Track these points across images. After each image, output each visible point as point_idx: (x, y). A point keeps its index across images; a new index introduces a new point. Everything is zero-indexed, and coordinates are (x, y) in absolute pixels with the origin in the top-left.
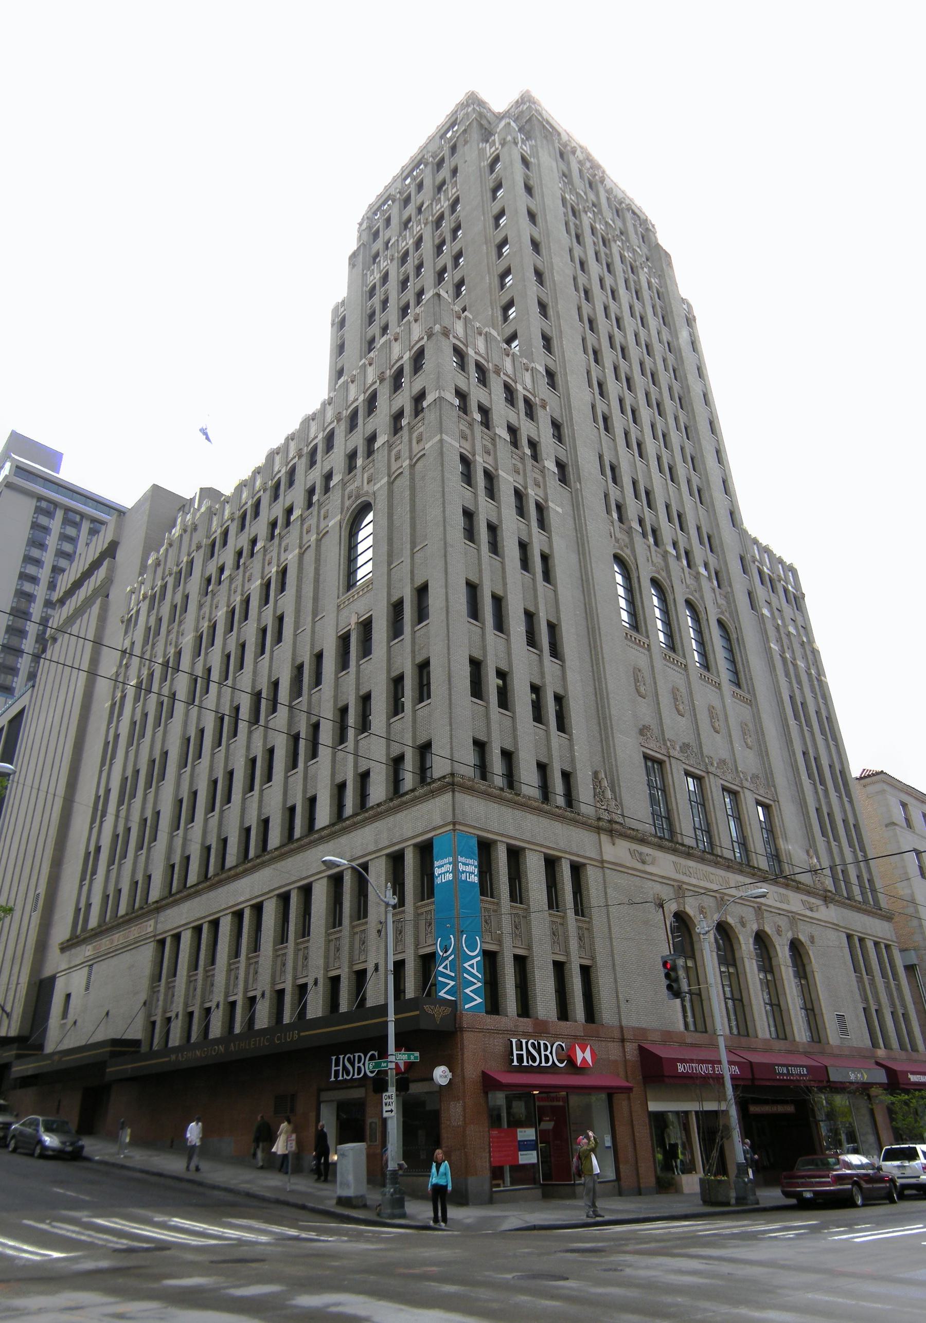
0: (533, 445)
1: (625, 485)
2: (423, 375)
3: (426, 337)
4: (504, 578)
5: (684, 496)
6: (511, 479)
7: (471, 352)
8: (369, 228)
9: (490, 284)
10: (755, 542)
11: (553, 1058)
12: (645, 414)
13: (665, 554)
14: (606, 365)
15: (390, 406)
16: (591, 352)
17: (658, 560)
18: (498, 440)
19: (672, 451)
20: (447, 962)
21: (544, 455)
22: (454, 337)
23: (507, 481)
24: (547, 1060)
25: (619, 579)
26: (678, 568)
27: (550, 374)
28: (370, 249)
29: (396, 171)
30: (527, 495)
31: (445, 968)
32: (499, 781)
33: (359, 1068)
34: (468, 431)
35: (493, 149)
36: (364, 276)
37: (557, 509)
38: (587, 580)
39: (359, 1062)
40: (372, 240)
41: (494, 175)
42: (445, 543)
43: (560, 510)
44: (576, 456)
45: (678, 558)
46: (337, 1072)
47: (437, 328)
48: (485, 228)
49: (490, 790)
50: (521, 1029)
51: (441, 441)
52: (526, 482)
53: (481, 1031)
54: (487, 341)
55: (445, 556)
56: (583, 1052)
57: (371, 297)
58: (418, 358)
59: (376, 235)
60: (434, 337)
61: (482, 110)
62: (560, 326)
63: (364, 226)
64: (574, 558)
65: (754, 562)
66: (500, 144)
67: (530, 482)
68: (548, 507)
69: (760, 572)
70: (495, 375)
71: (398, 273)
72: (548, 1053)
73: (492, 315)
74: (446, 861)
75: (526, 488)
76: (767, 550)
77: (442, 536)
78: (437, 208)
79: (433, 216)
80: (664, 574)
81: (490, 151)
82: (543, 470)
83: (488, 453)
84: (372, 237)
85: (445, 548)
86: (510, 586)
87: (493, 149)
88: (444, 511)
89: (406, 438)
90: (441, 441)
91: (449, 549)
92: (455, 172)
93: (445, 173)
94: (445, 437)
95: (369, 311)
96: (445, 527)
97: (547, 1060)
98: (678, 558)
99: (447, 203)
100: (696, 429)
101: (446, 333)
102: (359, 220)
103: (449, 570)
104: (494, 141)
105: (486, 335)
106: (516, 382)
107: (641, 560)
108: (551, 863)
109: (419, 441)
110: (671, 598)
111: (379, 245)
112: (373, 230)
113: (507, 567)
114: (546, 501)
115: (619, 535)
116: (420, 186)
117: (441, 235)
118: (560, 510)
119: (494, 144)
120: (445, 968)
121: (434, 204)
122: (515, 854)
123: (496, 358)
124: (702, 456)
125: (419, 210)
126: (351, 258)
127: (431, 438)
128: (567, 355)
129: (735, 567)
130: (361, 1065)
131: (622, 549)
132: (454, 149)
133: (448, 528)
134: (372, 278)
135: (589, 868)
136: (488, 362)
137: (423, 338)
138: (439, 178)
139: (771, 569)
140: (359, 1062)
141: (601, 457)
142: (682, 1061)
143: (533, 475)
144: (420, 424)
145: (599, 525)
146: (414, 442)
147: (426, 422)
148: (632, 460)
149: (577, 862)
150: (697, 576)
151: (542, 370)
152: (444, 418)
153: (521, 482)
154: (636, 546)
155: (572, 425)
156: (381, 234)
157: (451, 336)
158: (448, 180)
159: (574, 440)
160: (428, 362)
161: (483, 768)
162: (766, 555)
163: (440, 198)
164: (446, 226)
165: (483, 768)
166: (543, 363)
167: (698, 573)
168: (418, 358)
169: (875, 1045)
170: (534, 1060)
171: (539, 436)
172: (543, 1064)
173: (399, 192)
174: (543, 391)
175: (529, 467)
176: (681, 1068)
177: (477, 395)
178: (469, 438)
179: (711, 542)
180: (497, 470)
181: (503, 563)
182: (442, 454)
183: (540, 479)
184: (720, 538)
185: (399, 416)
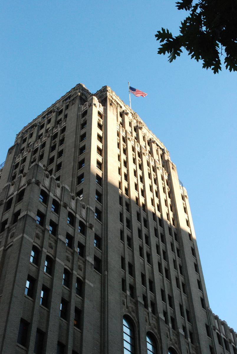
0: (81, 246)
1: (136, 276)
2: (21, 204)
3: (27, 184)
4: (48, 321)
5: (173, 287)
6: (63, 264)
7: (51, 195)
8: (22, 137)
9: (74, 166)
10: (216, 318)
12: (154, 240)
13: (158, 319)
14: (133, 212)
15: (2, 218)
16: (124, 204)
17: (153, 322)
18: (59, 242)
19: (168, 262)
21: (87, 253)
23: (61, 263)
25: (126, 330)
26: (165, 329)
27: (98, 212)
28: (21, 146)
29: (40, 113)
30: (72, 274)
34: (41, 234)
35: (85, 108)
36: (14, 158)
37: (92, 283)
38: (104, 329)
40: (22, 143)
41: (84, 118)
42: (12, 295)
43: (92, 285)
44: (107, 257)
45: (166, 322)
47: (34, 180)
48: (75, 141)
51: (22, 237)
52: (73, 267)
54: (62, 191)
55: (10, 303)
57: (15, 169)
58: (21, 196)
59: (25, 141)
60: (30, 185)
61: (84, 92)
62: (107, 189)
63: (20, 136)
64: (97, 314)
65: (215, 330)
66: (88, 106)
67: (75, 267)
68: (85, 282)
69: (219, 336)
70: (64, 208)
71: (31, 158)
73: (72, 181)
75: (72, 270)
76: (224, 324)
77: (11, 291)
78: (55, 131)
79: (52, 134)
80: (156, 331)
81: (83, 108)
82: (85, 262)
83: (51, 247)
84: (22, 141)
85: (11, 298)
86: (50, 326)
87: (85, 108)
88: (15, 277)
89: (5, 235)
90: (22, 237)
91: (14, 299)
92: (66, 116)
93: (62, 116)
94: (25, 235)
95: (13, 175)
96: (14, 285)
98: (166, 322)
99: (60, 129)
100: (183, 252)
101: (38, 183)
102: (18, 133)
103: (11, 312)
104: (86, 104)
105: (62, 188)
106: (76, 213)
107: (142, 320)
109: (12, 237)
110: (160, 346)
111: (25, 145)
112: (23, 138)
113: (51, 315)
114: (84, 279)
115: (130, 305)
116: (49, 121)
117: (55, 142)
118: (92, 285)
119: (86, 106)
121: (54, 129)
123: (66, 199)
124: (186, 266)
125: (47, 131)
126: (9, 150)
127: (17, 236)
128: (109, 204)
129: (202, 331)
131: (130, 313)
132: (67, 107)
133: (16, 286)
134: (18, 159)
136: (61, 201)
137: (25, 185)
138: (59, 118)
139: (226, 336)
141: (123, 259)
143: (78, 262)
144: (14, 228)
145: (114, 296)
146: (9, 237)
147: (17, 227)
148: (142, 263)
150: (178, 335)
151: (93, 209)
152: (27, 225)
153: (70, 266)
154: (139, 312)
155: (107, 240)
156: (27, 140)
158: (62, 120)
159: (107, 248)
160: (26, 197)
162: (223, 327)
163: (57, 126)
164: (57, 139)
166: (95, 206)
167: (178, 333)
168: (21, 196)
171: (85, 243)
173: (39, 123)
174: (93, 219)
175: (76, 259)
177: (51, 216)
179: (190, 315)
180: (55, 258)
181: (49, 312)
182: (21, 245)
183: (82, 266)
184: (194, 314)
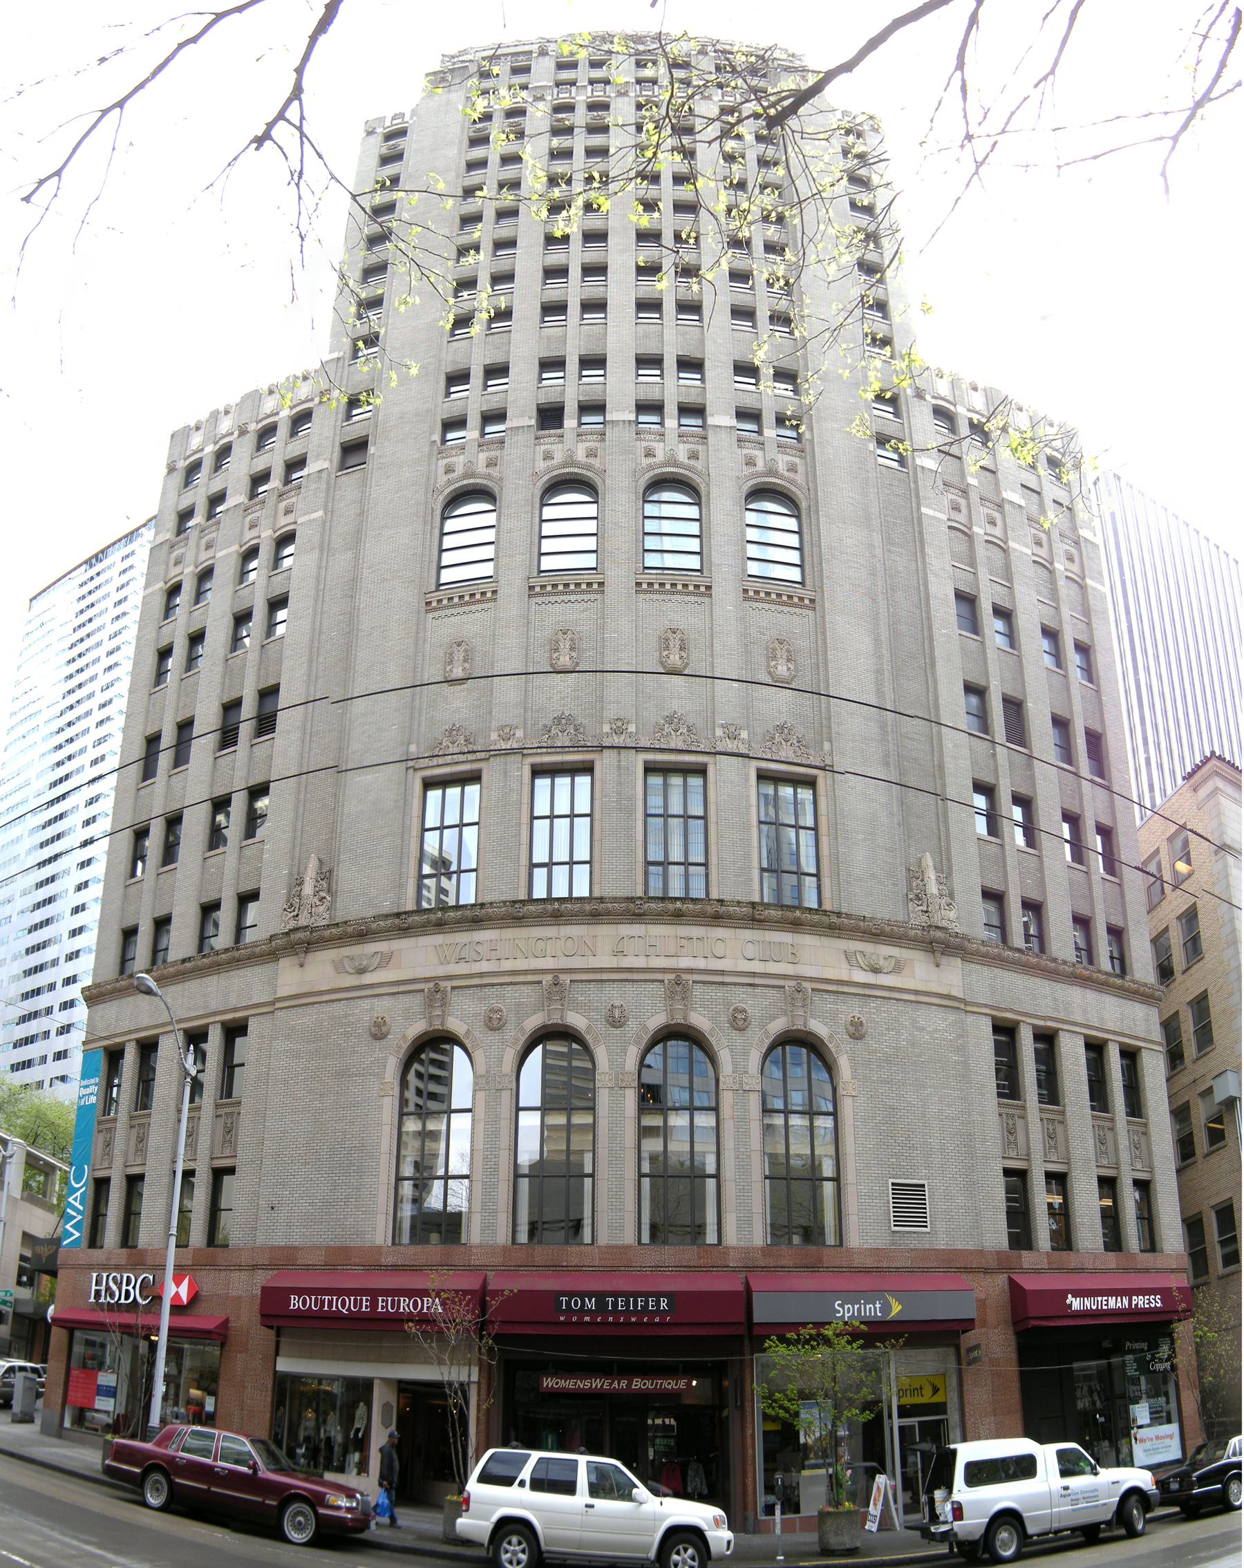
11: (135, 1294)
20: (78, 1194)
22: (934, 397)
24: (127, 1297)
31: (75, 1199)
32: (1105, 964)
33: (127, 1292)
39: (128, 1285)
46: (98, 1293)
49: (1095, 975)
50: (112, 1262)
53: (73, 1267)
56: (178, 1284)
72: (130, 1288)
74: (93, 1081)
97: (127, 1297)
108: (1095, 1049)
120: (75, 1199)
122: (1047, 1039)
130: (130, 1288)
135: (1144, 1054)
140: (128, 1285)
142: (299, 1292)
149: (1129, 1045)
157: (928, 397)
161: (1088, 951)
165: (1088, 951)
169: (1021, 1234)
170: (112, 1295)
172: (122, 1301)
176: (295, 1303)
178: (1076, 558)
185: (260, 478)
